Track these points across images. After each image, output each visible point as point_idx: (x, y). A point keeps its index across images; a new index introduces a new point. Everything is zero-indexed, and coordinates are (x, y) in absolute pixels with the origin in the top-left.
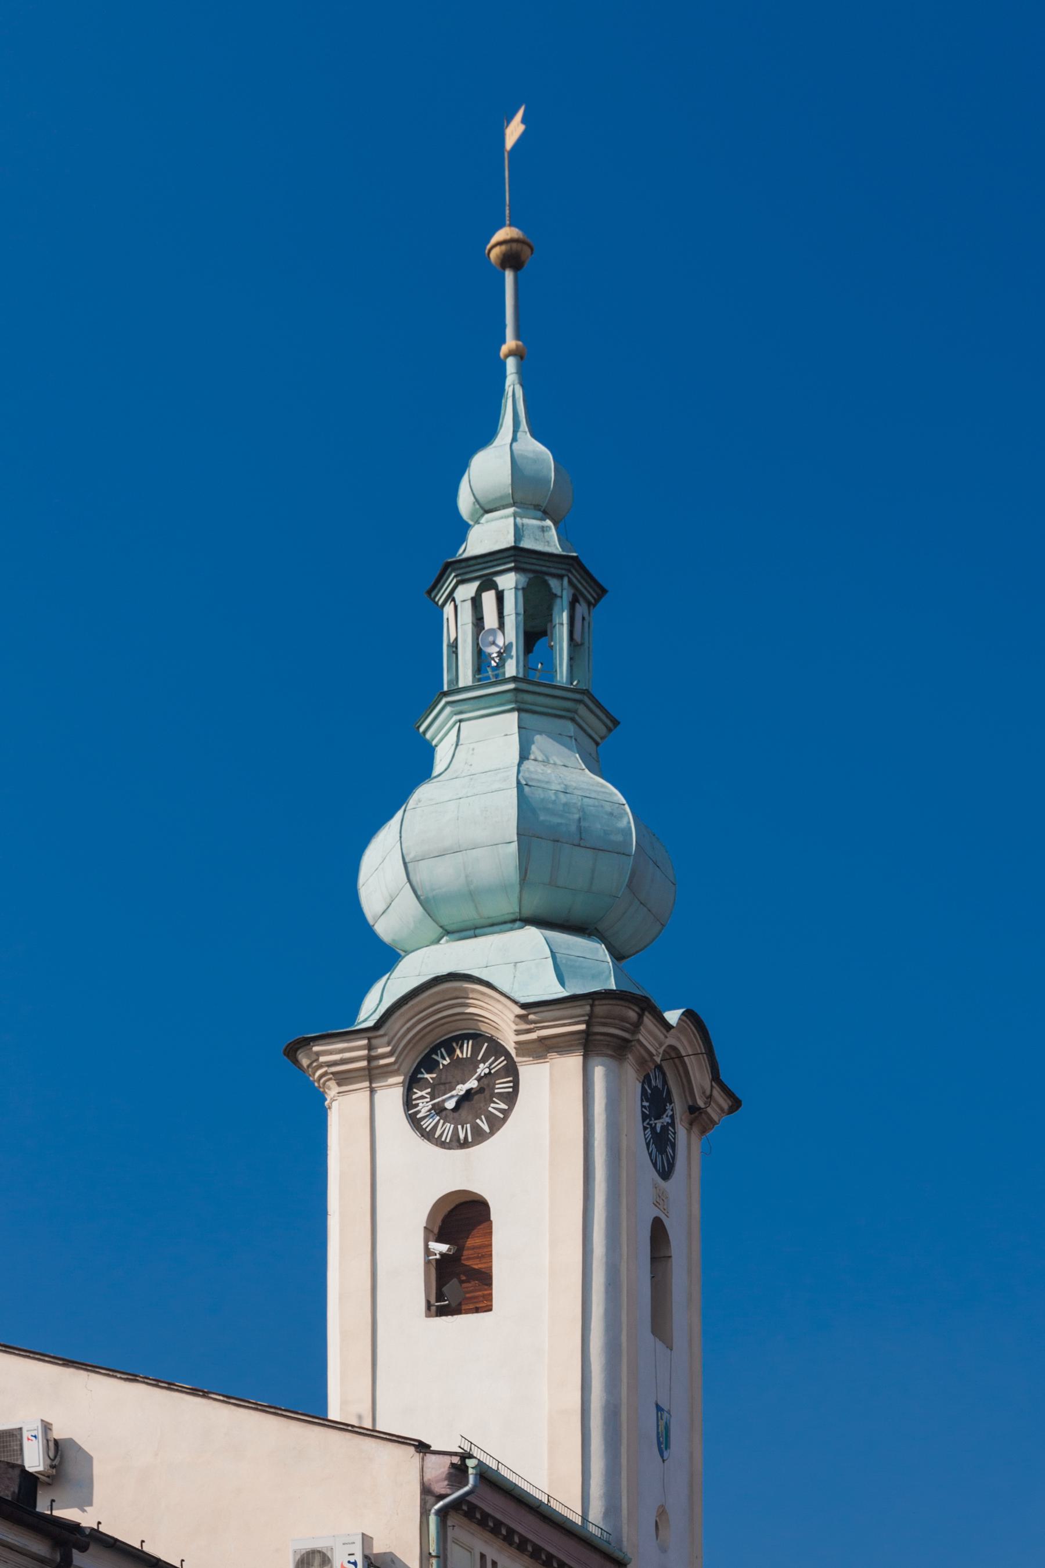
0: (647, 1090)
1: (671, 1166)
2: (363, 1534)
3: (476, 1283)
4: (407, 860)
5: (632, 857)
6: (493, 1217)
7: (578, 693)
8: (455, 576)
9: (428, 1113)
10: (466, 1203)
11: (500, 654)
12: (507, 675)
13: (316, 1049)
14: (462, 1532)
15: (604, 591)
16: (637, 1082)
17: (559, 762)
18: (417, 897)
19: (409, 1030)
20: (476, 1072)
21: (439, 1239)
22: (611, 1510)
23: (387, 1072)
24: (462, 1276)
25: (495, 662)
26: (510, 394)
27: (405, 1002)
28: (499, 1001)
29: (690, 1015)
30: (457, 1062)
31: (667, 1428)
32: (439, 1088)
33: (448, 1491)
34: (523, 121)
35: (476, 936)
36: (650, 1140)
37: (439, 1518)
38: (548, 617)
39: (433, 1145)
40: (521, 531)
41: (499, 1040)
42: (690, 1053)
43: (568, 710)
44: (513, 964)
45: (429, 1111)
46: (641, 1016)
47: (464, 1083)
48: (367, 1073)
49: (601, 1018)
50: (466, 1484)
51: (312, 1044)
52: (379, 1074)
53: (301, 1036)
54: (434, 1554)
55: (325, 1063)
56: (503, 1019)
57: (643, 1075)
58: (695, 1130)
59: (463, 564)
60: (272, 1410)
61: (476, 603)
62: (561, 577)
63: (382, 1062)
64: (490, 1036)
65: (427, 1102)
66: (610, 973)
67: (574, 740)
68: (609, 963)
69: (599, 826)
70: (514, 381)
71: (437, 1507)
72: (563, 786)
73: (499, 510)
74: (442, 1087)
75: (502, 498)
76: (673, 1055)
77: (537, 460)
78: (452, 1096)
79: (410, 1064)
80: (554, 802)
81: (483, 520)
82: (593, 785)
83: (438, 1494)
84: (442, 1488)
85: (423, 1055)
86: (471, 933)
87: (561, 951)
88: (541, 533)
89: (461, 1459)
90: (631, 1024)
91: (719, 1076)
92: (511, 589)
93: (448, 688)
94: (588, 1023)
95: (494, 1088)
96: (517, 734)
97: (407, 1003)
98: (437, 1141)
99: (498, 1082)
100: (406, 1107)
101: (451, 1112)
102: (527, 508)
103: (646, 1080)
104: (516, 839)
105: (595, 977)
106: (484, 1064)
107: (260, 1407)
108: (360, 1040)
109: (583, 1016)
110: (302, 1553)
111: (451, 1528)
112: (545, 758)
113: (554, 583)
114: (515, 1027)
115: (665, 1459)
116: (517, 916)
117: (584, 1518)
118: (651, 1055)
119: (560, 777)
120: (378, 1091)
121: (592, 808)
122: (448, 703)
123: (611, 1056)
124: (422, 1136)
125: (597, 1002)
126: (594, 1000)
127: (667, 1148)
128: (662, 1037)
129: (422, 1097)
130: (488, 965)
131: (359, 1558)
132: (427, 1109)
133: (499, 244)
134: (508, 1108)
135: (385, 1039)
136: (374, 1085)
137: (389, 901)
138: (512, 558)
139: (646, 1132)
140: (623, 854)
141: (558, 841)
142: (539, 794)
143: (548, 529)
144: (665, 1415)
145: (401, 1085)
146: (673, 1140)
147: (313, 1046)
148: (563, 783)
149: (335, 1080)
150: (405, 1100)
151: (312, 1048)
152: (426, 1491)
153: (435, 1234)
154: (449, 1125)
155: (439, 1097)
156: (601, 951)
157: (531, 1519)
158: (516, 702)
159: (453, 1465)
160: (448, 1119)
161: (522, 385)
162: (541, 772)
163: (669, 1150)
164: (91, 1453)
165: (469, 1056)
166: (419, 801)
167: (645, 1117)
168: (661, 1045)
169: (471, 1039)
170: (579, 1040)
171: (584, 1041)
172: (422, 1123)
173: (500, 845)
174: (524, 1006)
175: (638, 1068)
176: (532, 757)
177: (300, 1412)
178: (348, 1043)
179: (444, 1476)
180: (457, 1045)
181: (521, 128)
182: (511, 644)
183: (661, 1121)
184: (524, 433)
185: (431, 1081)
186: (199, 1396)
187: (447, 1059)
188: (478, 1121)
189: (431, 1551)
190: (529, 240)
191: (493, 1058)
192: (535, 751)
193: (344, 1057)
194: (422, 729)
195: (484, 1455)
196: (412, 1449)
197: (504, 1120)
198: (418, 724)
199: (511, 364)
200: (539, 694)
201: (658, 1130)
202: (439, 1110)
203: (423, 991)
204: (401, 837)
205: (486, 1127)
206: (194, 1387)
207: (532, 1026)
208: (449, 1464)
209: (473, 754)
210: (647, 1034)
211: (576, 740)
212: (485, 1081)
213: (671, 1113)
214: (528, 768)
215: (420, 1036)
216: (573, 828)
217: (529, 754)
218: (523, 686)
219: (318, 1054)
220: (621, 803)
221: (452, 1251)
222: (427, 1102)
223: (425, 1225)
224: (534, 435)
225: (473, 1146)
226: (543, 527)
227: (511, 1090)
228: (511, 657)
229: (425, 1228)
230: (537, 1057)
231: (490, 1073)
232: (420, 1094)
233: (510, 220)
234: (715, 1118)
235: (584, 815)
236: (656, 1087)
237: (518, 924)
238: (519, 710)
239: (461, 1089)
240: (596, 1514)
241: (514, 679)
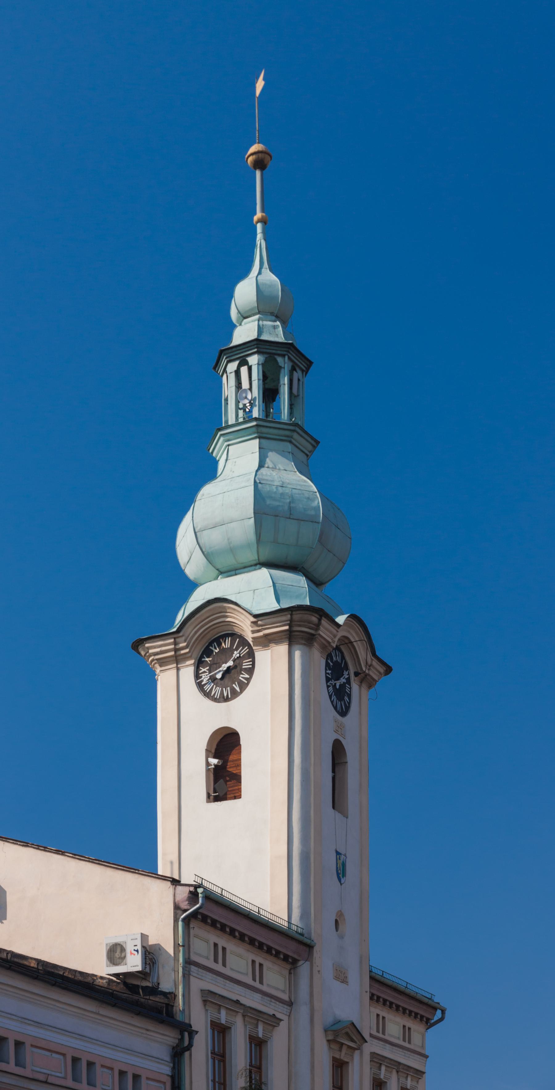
0: (330, 664)
1: (348, 708)
2: (142, 934)
3: (235, 782)
4: (196, 531)
5: (320, 524)
6: (241, 743)
7: (292, 425)
8: (226, 358)
9: (208, 682)
10: (228, 734)
11: (250, 402)
12: (254, 417)
13: (147, 645)
14: (197, 929)
15: (311, 363)
16: (322, 659)
17: (282, 468)
18: (203, 552)
19: (196, 632)
20: (233, 656)
21: (215, 757)
22: (305, 914)
24: (227, 778)
25: (248, 409)
26: (259, 246)
27: (193, 616)
28: (242, 614)
29: (353, 617)
30: (223, 651)
31: (344, 865)
32: (214, 666)
33: (188, 907)
34: (264, 79)
35: (236, 574)
36: (332, 693)
37: (184, 923)
38: (277, 380)
39: (210, 701)
40: (262, 329)
41: (245, 637)
42: (357, 640)
43: (288, 436)
44: (253, 591)
45: (208, 680)
46: (320, 620)
47: (226, 663)
48: (175, 658)
49: (298, 622)
50: (198, 903)
51: (145, 642)
52: (182, 659)
53: (138, 638)
54: (181, 944)
55: (153, 653)
56: (245, 624)
57: (326, 655)
58: (364, 685)
59: (230, 351)
60: (97, 862)
61: (238, 373)
62: (283, 356)
63: (183, 652)
64: (240, 634)
65: (207, 675)
66: (307, 594)
67: (291, 454)
68: (306, 588)
69: (301, 506)
70: (260, 238)
71: (182, 917)
72: (281, 483)
73: (251, 316)
74: (215, 666)
75: (252, 309)
76: (347, 641)
77: (272, 286)
78: (220, 671)
79: (198, 652)
80: (275, 493)
81: (243, 324)
82: (299, 481)
83: (183, 909)
84: (185, 906)
85: (205, 647)
86: (233, 573)
87: (279, 582)
88: (273, 330)
89: (194, 888)
90: (314, 625)
91: (376, 653)
92: (256, 364)
93: (224, 425)
94: (290, 625)
95: (242, 666)
96: (258, 454)
97: (194, 617)
98: (212, 698)
99: (244, 661)
100: (196, 678)
101: (220, 680)
102: (267, 315)
103: (329, 657)
104: (253, 515)
105: (298, 596)
106: (237, 651)
107: (91, 860)
108: (170, 640)
109: (287, 621)
110: (110, 945)
111: (192, 929)
112: (274, 466)
113: (280, 360)
114: (251, 629)
115: (342, 883)
116: (257, 562)
117: (289, 922)
118: (329, 643)
119: (280, 477)
120: (181, 669)
121: (297, 495)
122: (221, 435)
123: (305, 644)
124: (205, 695)
125: (294, 613)
126: (292, 611)
127: (344, 697)
128: (334, 631)
129: (205, 672)
130: (240, 592)
131: (139, 948)
132: (207, 679)
133: (252, 154)
134: (250, 677)
135: (183, 638)
136: (179, 666)
137: (190, 555)
138: (256, 346)
139: (329, 689)
140: (315, 522)
141: (277, 516)
142: (267, 488)
143: (277, 327)
144: (342, 857)
145: (193, 665)
146: (349, 693)
147: (145, 644)
148: (281, 481)
149: (158, 663)
150: (195, 674)
151: (145, 645)
152: (177, 907)
153: (213, 753)
154: (218, 688)
155: (213, 672)
156: (303, 581)
157: (246, 922)
158: (258, 433)
159: (190, 892)
160: (218, 685)
161: (265, 240)
162: (270, 474)
163: (346, 698)
164: (6, 889)
165: (229, 647)
166: (203, 495)
167: (328, 680)
168: (335, 636)
169: (230, 636)
170: (285, 635)
171: (288, 636)
172: (205, 688)
173: (245, 520)
174: (256, 616)
175: (321, 650)
176: (266, 466)
177: (111, 862)
178: (163, 641)
179: (186, 898)
180: (223, 640)
181: (263, 83)
182: (255, 398)
183: (339, 681)
184: (266, 269)
185: (209, 662)
186: (59, 854)
187: (218, 649)
188: (234, 685)
189: (180, 943)
190: (269, 151)
191: (241, 648)
192: (268, 462)
193: (162, 650)
194: (211, 451)
195: (212, 885)
196: (169, 883)
197: (248, 684)
198: (209, 448)
199: (259, 227)
200: (270, 427)
201: (338, 687)
202: (213, 679)
203: (203, 609)
204: (193, 517)
205: (238, 689)
206: (57, 849)
207: (260, 628)
208: (188, 892)
209: (235, 465)
210: (324, 630)
211: (292, 454)
212: (237, 661)
213: (347, 677)
214: (262, 473)
215: (202, 636)
216: (286, 508)
217: (265, 464)
218: (261, 423)
219: (149, 648)
220: (314, 491)
221: (220, 763)
222: (207, 675)
223: (206, 748)
224: (271, 270)
225: (231, 700)
226: (274, 326)
227: (251, 666)
228: (256, 406)
229: (206, 750)
230: (264, 646)
231: (240, 656)
232: (203, 670)
233: (259, 140)
234: (376, 677)
235: (293, 500)
236: (337, 661)
237: (258, 566)
238: (260, 438)
239: (224, 667)
240: (296, 919)
241: (256, 419)
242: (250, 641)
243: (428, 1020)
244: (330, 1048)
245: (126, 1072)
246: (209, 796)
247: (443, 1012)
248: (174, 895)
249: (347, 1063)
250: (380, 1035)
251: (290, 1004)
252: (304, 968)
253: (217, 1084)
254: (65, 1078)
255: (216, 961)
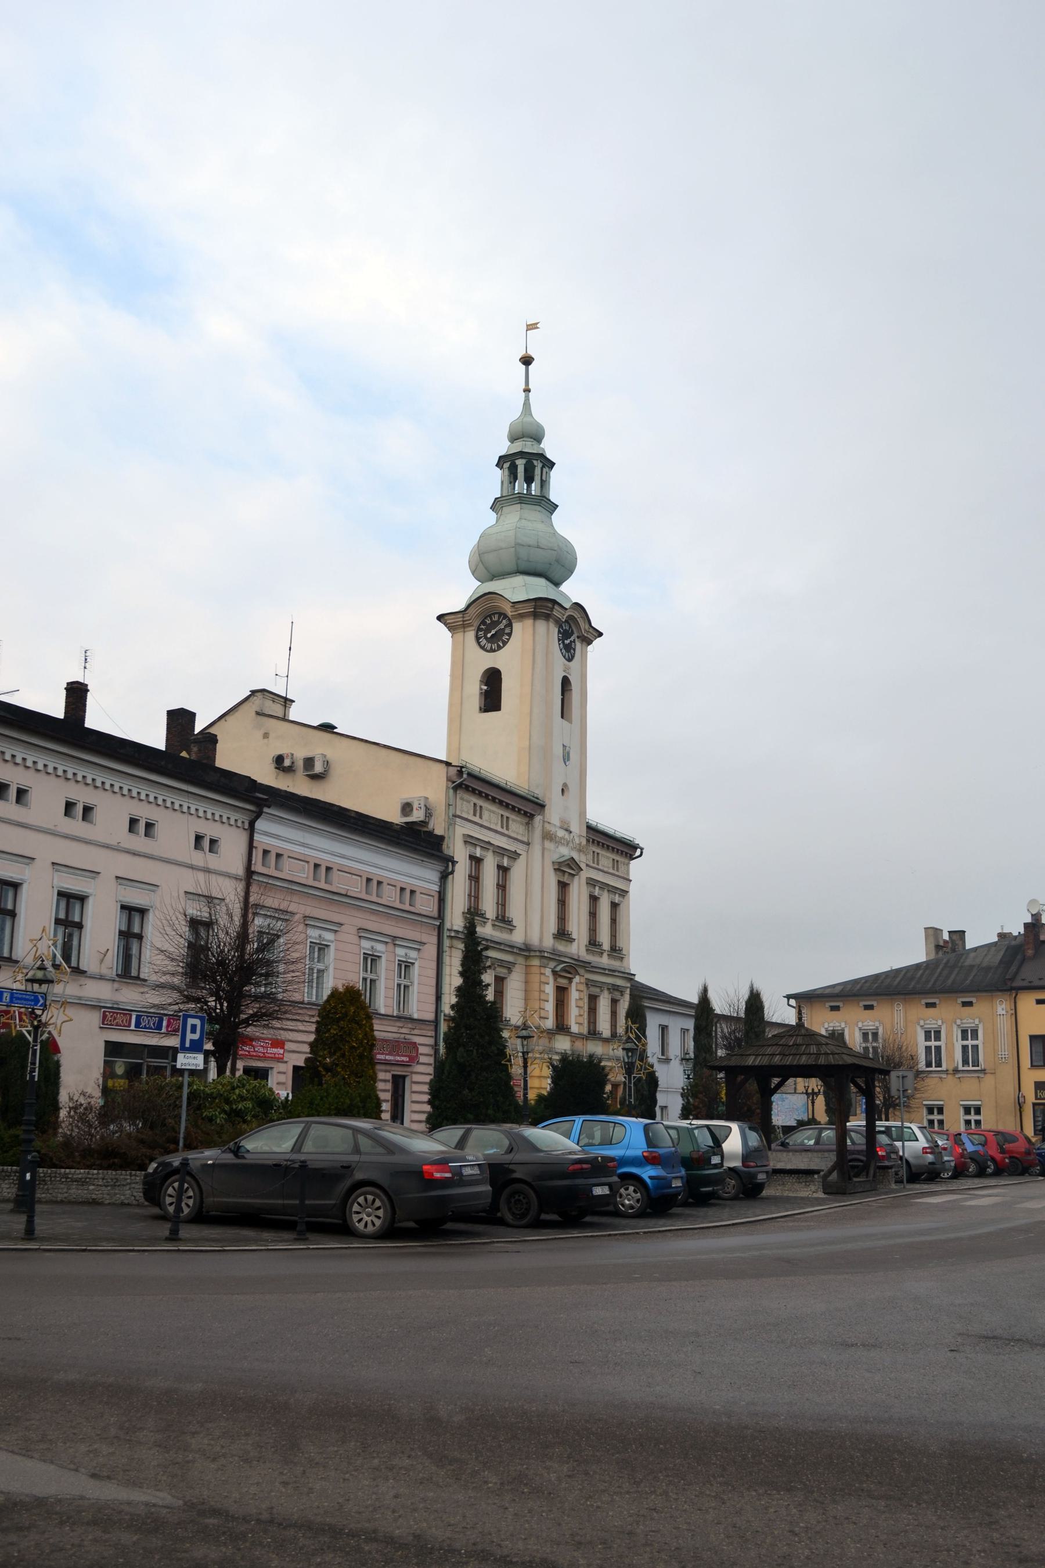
23: (470, 625)
31: (568, 753)
62: (537, 460)
131: (422, 806)
152: (449, 779)
163: (572, 651)
168: (564, 615)
205: (502, 645)
242: (510, 617)
243: (631, 855)
244: (556, 874)
245: (405, 889)
246: (480, 709)
247: (642, 849)
248: (447, 773)
249: (569, 884)
250: (595, 865)
251: (528, 844)
252: (538, 819)
253: (473, 898)
254: (395, 901)
255: (475, 815)
